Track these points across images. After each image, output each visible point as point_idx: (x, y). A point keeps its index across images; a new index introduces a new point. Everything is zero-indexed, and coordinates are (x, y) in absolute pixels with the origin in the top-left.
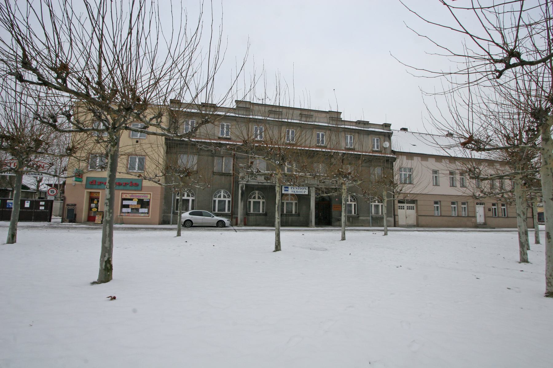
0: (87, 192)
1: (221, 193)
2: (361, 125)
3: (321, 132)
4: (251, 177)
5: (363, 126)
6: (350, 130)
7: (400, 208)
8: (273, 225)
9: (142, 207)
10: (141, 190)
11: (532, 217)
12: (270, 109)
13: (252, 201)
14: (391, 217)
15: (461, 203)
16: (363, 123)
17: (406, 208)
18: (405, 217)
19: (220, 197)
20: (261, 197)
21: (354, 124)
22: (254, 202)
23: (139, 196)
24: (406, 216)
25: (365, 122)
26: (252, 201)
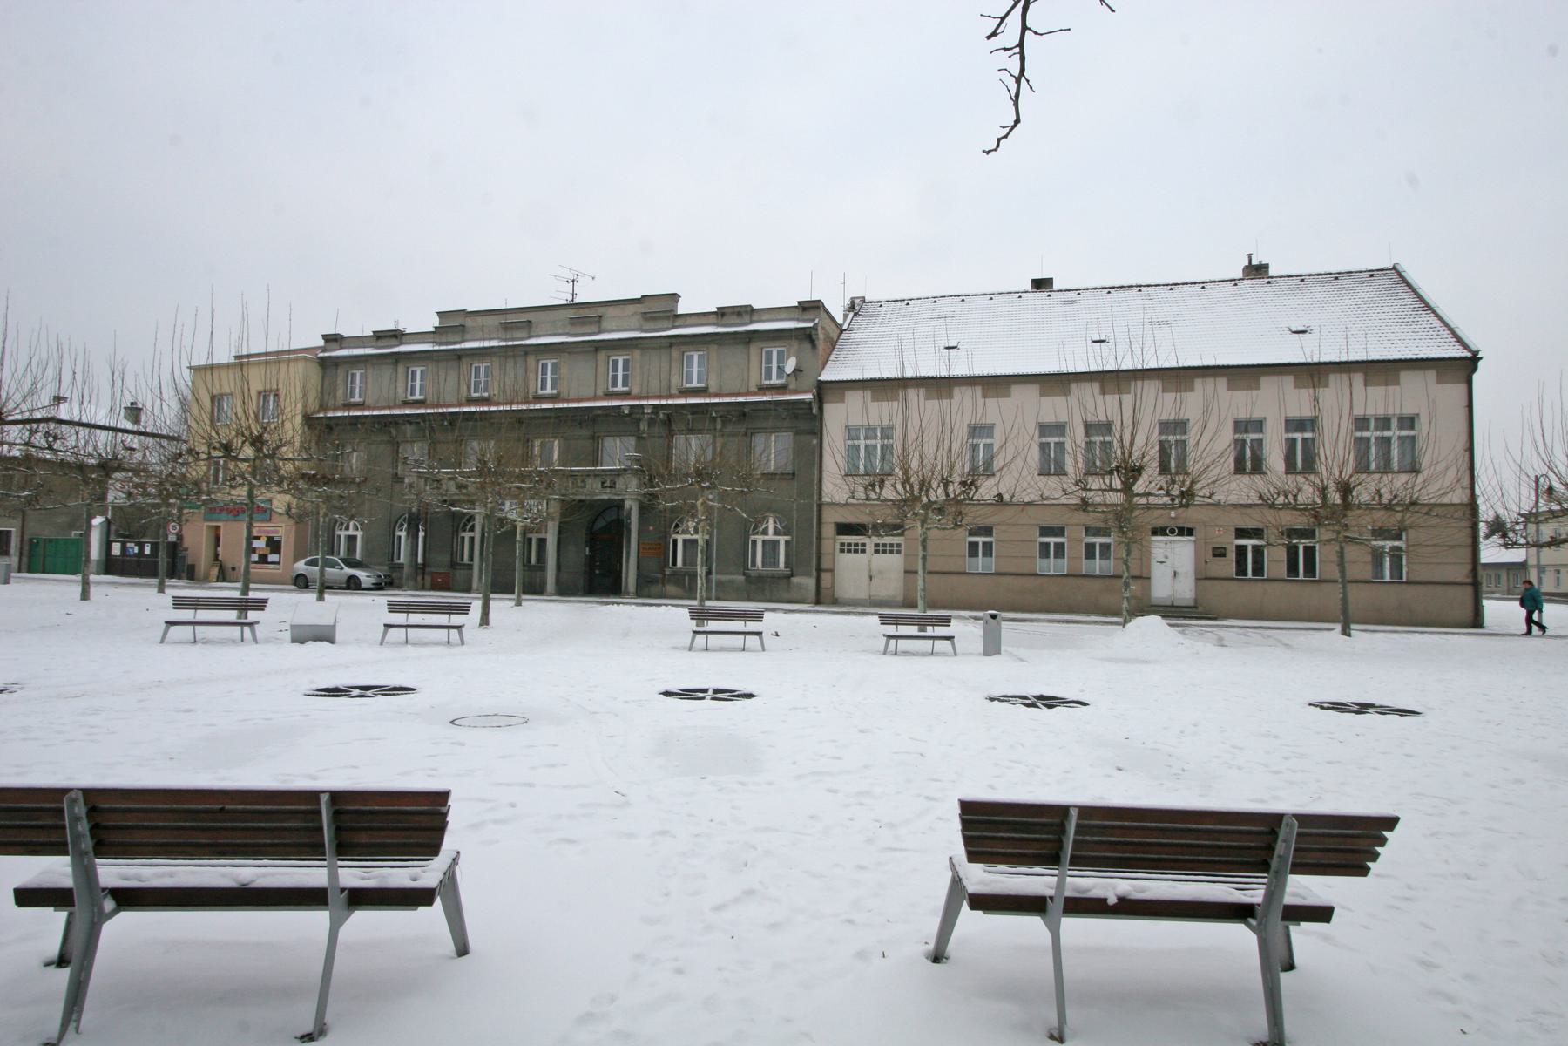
0: (208, 526)
1: (768, 522)
2: (726, 320)
3: (775, 347)
4: (430, 485)
5: (738, 321)
6: (688, 340)
7: (846, 548)
8: (513, 592)
9: (271, 553)
10: (270, 520)
11: (1469, 580)
12: (571, 313)
13: (680, 539)
14: (809, 575)
15: (1233, 529)
16: (733, 313)
17: (870, 548)
18: (866, 577)
19: (765, 532)
20: (471, 524)
21: (712, 319)
22: (685, 541)
23: (268, 532)
24: (870, 571)
25: (739, 309)
26: (760, 538)
